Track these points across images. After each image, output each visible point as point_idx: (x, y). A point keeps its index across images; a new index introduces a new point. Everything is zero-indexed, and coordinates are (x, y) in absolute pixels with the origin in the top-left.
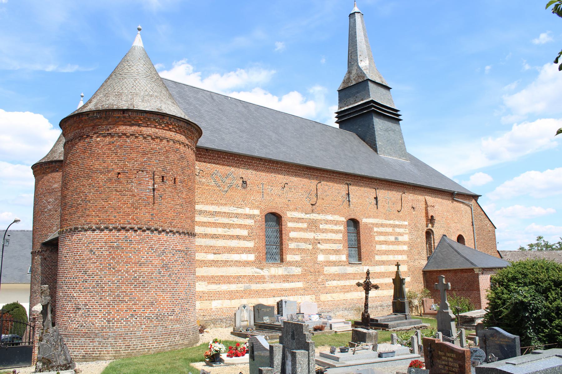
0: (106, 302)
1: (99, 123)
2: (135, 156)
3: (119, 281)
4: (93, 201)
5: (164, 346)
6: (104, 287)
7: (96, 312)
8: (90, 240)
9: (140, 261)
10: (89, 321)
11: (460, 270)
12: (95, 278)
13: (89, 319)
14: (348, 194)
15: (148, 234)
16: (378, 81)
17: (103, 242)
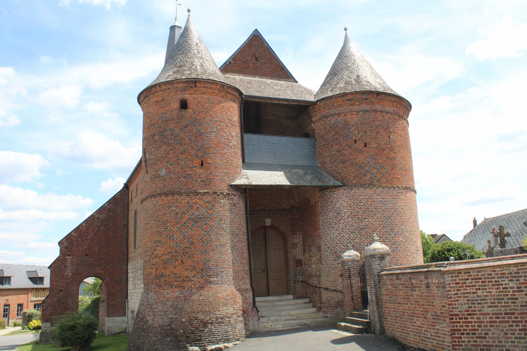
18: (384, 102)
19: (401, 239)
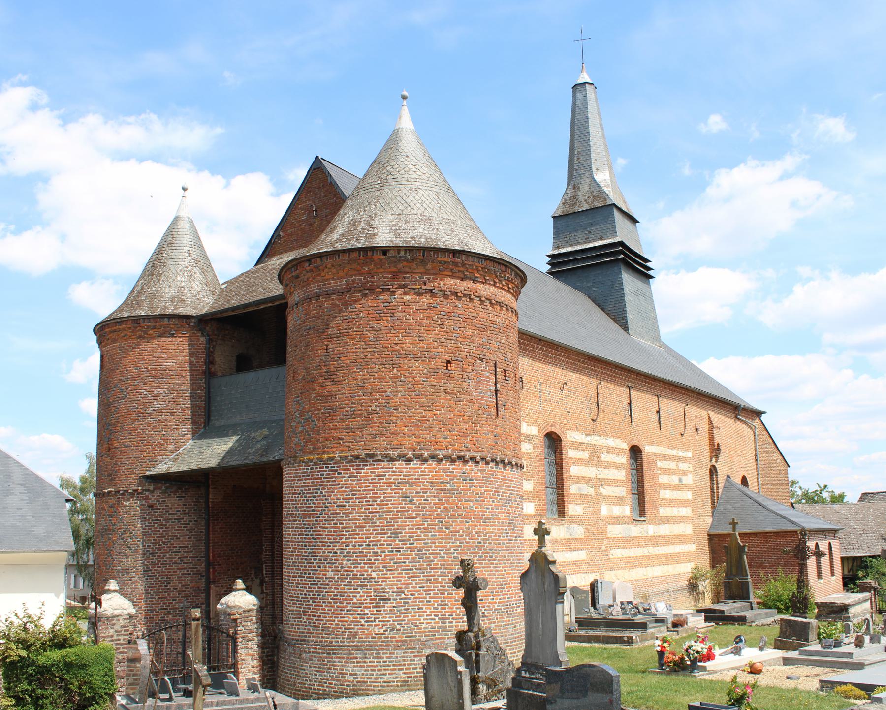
0: (437, 587)
1: (407, 269)
2: (471, 334)
3: (458, 550)
4: (403, 407)
6: (433, 561)
7: (421, 604)
8: (402, 477)
9: (484, 515)
10: (408, 620)
11: (774, 533)
12: (415, 545)
13: (407, 617)
14: (630, 404)
15: (492, 468)
16: (624, 209)
17: (427, 482)
18: (323, 274)
19: (330, 574)
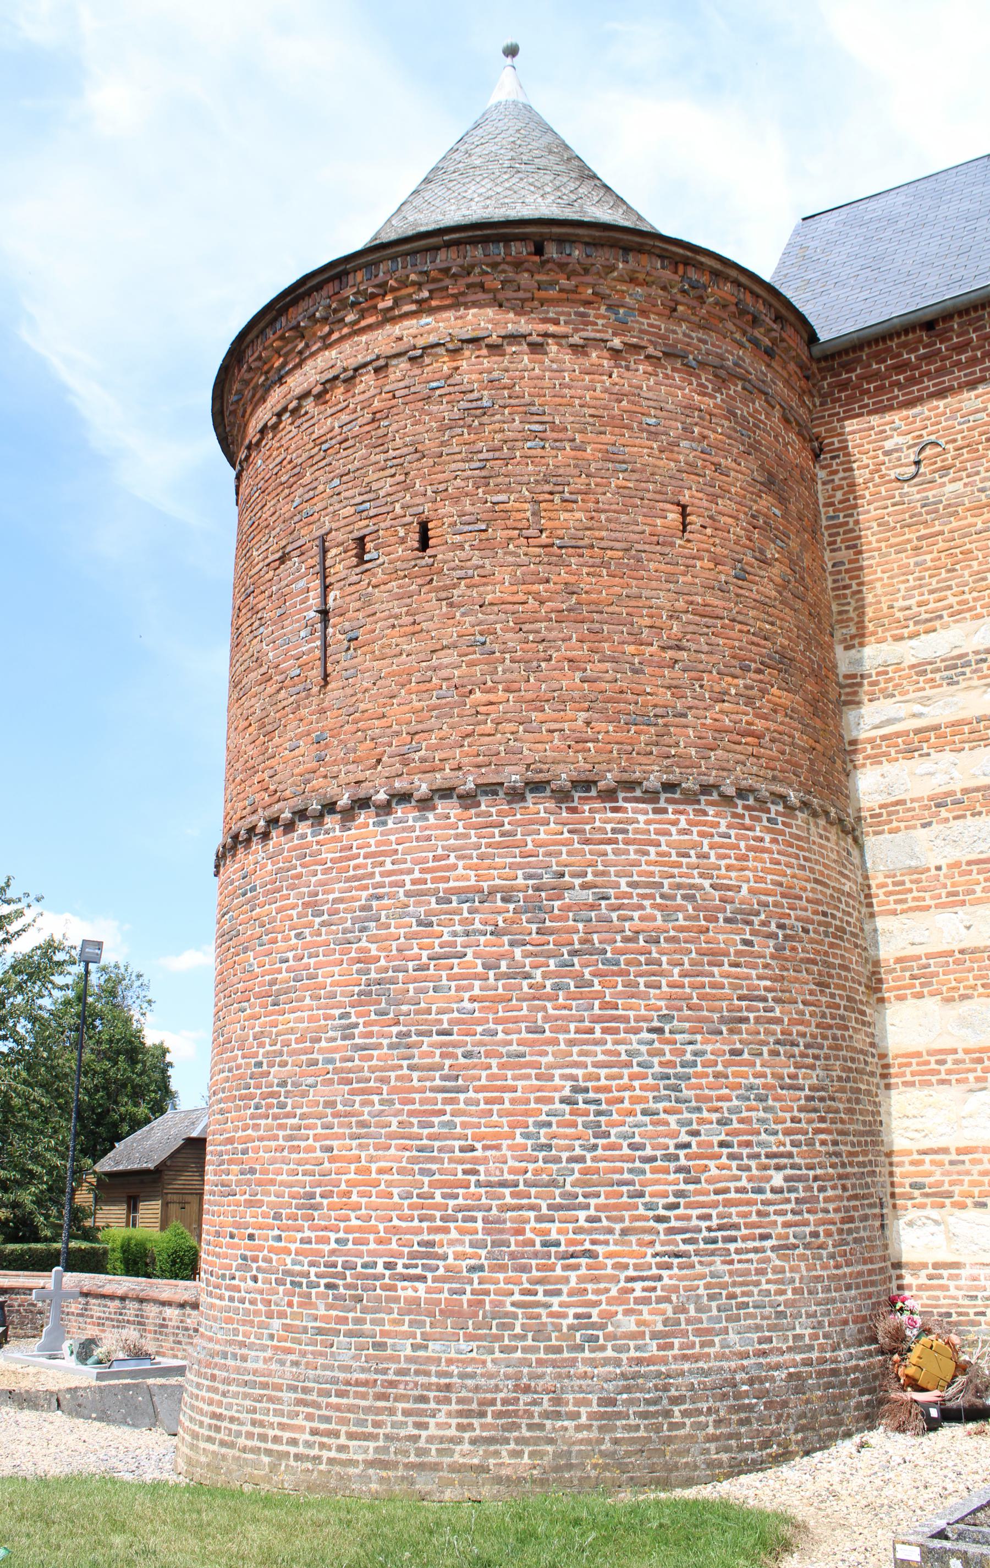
5: (343, 1456)
